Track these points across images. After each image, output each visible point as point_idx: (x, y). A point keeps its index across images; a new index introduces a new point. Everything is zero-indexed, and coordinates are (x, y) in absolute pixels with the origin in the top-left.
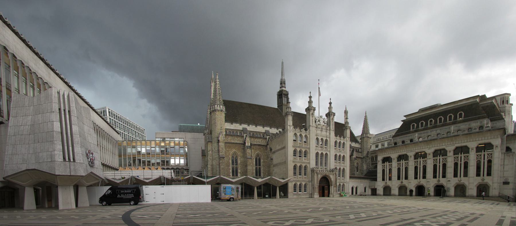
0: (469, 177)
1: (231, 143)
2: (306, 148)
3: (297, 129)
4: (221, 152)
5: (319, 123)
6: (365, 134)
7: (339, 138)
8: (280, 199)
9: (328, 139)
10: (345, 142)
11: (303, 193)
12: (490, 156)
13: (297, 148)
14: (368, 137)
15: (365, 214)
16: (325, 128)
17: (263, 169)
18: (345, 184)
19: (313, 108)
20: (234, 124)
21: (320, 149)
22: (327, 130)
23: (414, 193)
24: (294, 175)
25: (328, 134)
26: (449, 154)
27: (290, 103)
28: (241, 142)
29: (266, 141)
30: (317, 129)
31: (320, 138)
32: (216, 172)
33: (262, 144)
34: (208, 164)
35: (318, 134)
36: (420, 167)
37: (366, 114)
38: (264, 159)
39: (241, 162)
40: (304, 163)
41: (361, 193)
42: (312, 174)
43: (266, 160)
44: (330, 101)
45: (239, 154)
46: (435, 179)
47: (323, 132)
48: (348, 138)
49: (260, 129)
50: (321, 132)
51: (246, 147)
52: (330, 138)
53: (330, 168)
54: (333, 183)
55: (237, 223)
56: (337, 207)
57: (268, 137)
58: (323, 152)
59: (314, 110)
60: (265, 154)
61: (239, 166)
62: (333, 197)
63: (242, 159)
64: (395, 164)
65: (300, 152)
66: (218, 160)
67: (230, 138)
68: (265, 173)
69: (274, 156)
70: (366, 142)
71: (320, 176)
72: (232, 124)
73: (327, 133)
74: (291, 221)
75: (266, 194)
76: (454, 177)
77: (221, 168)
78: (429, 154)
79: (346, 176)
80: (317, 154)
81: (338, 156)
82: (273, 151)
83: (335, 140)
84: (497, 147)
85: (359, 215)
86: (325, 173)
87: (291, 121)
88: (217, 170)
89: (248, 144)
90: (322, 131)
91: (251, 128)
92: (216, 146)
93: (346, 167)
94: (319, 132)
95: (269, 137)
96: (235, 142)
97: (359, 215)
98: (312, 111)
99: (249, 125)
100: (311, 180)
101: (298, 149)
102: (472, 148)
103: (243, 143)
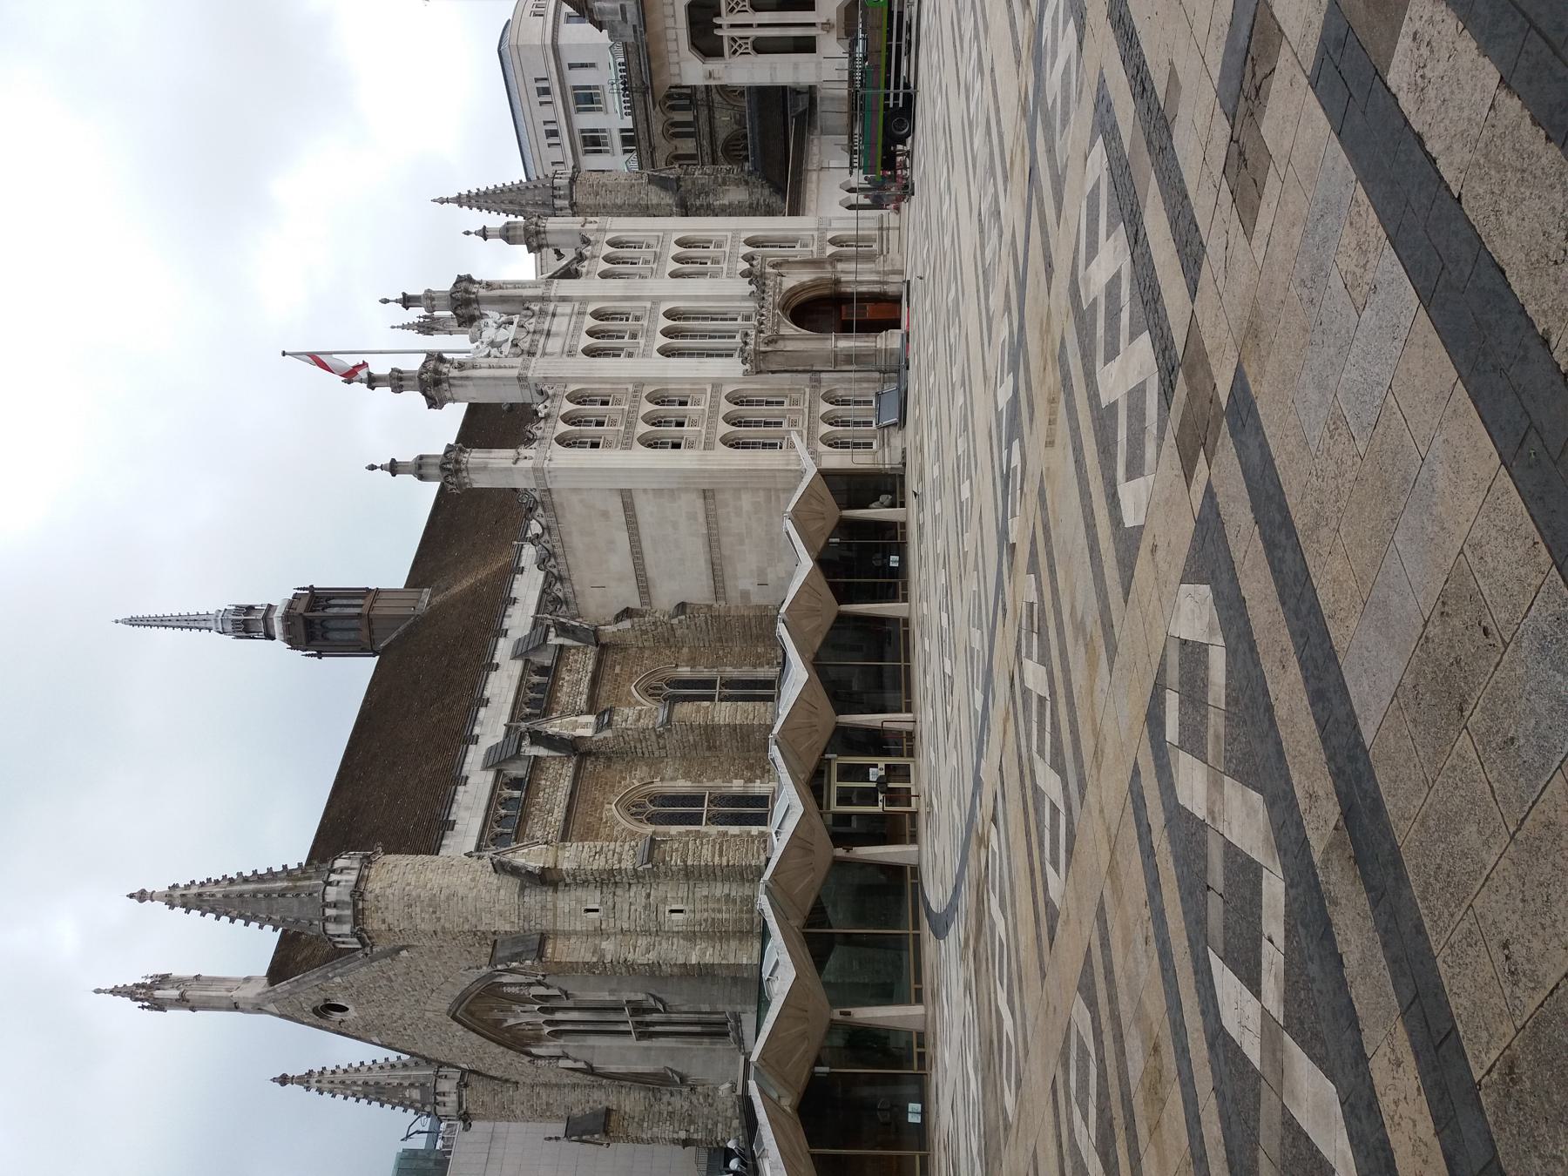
1: (567, 820)
2: (635, 396)
3: (534, 430)
5: (506, 348)
6: (554, 197)
7: (586, 263)
9: (591, 308)
10: (609, 236)
13: (641, 414)
14: (573, 180)
16: (533, 320)
18: (830, 235)
19: (431, 365)
21: (641, 341)
22: (543, 313)
24: (781, 448)
25: (565, 308)
27: (393, 460)
28: (569, 770)
29: (573, 651)
30: (539, 352)
33: (590, 668)
34: (681, 961)
35: (566, 349)
36: (760, 25)
37: (447, 201)
39: (686, 776)
40: (714, 407)
42: (774, 368)
43: (685, 650)
44: (396, 301)
45: (635, 780)
46: (820, 44)
47: (554, 329)
48: (588, 226)
49: (502, 685)
50: (557, 335)
51: (601, 735)
52: (585, 300)
53: (743, 298)
54: (827, 273)
55: (1042, 864)
56: (965, 554)
57: (553, 640)
58: (661, 328)
59: (439, 358)
60: (647, 653)
63: (669, 772)
65: (657, 422)
68: (758, 656)
70: (597, 194)
71: (789, 329)
73: (559, 310)
74: (1040, 782)
75: (879, 563)
79: (790, 233)
80: (666, 352)
81: (668, 340)
82: (635, 603)
83: (597, 277)
86: (772, 312)
87: (492, 455)
89: (585, 726)
90: (549, 331)
91: (492, 726)
92: (578, 901)
93: (737, 231)
94: (554, 345)
95: (552, 635)
96: (563, 805)
98: (445, 370)
99: (475, 740)
100: (807, 376)
101: (642, 428)
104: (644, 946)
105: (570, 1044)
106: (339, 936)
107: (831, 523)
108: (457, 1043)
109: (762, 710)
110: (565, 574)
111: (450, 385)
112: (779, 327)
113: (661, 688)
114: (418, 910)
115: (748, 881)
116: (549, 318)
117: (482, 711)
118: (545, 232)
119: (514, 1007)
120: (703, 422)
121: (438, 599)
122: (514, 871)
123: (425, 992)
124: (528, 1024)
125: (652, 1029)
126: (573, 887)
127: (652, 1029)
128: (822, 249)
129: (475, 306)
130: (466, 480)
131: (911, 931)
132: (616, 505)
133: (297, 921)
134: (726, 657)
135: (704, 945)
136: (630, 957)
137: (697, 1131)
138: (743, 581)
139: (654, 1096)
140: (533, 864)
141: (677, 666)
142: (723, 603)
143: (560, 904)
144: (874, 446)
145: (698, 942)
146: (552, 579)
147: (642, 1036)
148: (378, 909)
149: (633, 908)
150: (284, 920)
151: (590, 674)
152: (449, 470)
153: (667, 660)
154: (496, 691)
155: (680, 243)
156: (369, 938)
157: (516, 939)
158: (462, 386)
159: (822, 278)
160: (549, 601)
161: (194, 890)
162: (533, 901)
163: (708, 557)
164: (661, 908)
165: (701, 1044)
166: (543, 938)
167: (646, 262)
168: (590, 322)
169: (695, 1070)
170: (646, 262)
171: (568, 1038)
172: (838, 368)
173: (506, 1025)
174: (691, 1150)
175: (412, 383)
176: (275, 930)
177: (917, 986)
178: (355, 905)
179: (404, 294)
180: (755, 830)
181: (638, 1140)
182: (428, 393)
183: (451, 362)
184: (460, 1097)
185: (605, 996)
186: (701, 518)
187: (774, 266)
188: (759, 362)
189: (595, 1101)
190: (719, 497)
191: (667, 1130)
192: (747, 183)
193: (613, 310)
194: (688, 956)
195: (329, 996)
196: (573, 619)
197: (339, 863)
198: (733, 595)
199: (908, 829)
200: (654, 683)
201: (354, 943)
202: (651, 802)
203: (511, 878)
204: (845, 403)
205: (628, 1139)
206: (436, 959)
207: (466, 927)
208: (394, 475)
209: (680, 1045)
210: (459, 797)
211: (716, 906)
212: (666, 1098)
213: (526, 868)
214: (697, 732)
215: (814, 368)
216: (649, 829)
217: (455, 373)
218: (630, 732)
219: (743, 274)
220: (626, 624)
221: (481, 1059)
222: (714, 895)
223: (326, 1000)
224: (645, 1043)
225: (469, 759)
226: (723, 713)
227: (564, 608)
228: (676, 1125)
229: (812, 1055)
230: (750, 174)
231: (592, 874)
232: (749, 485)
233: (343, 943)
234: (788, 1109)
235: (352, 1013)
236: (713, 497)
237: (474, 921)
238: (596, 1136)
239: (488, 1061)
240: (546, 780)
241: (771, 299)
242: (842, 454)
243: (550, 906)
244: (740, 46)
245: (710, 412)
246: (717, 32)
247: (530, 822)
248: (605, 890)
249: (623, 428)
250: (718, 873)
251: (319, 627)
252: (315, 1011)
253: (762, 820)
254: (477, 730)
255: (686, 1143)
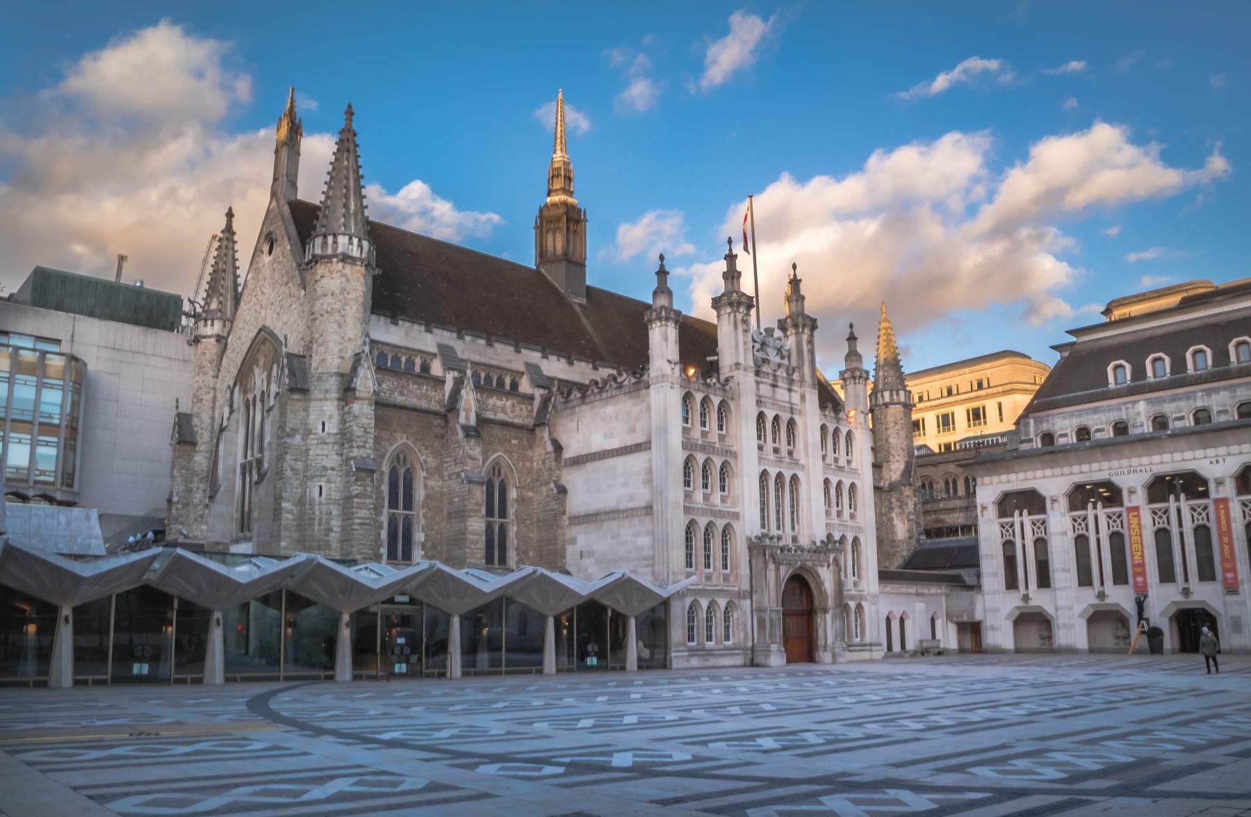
0: (1055, 590)
2: (726, 452)
4: (359, 447)
5: (760, 355)
6: (891, 392)
7: (832, 414)
8: (83, 693)
11: (721, 646)
12: (1200, 514)
15: (761, 746)
16: (785, 375)
17: (517, 533)
19: (743, 299)
20: (404, 325)
22: (791, 382)
23: (442, 670)
25: (796, 398)
26: (1217, 492)
28: (434, 406)
29: (529, 408)
30: (759, 379)
31: (770, 415)
32: (327, 535)
34: (284, 495)
35: (763, 399)
38: (523, 487)
40: (720, 514)
41: (925, 645)
42: (754, 562)
44: (795, 275)
46: (1013, 593)
47: (778, 390)
50: (774, 392)
58: (783, 471)
61: (421, 515)
62: (834, 662)
64: (1059, 522)
66: (338, 480)
67: (389, 383)
68: (526, 553)
69: (574, 480)
70: (896, 423)
71: (785, 572)
72: (431, 332)
73: (793, 394)
76: (1081, 584)
77: (357, 521)
78: (1219, 483)
80: (764, 475)
82: (568, 454)
83: (822, 423)
84: (1054, 501)
85: (783, 743)
88: (330, 530)
89: (467, 418)
90: (777, 386)
92: (331, 417)
94: (765, 390)
97: (783, 743)
98: (741, 310)
99: (460, 337)
102: (1051, 497)
103: (442, 410)
104: (296, 467)
105: (240, 415)
106: (314, 246)
107: (622, 608)
108: (245, 333)
109: (478, 556)
110: (587, 400)
111: (729, 314)
112: (787, 564)
113: (499, 475)
114: (330, 301)
115: (342, 546)
116: (787, 386)
117: (482, 342)
118: (855, 383)
119: (265, 373)
120: (707, 505)
121: (578, 309)
122: (354, 369)
123: (278, 308)
124: (255, 383)
125: (247, 475)
126: (342, 413)
127: (247, 475)
128: (853, 598)
129: (794, 332)
130: (654, 326)
131: (282, 674)
132: (639, 438)
133: (325, 216)
134: (525, 526)
135: (295, 512)
136: (288, 457)
137: (177, 509)
138: (583, 540)
139: (203, 478)
140: (358, 383)
141: (517, 488)
142: (567, 523)
143: (329, 403)
144: (690, 644)
145: (298, 508)
146: (582, 388)
147: (243, 467)
148: (331, 272)
149: (324, 458)
150: (327, 207)
151: (510, 420)
152: (661, 313)
153: (522, 480)
154: (499, 351)
155: (853, 486)
156: (311, 267)
157: (305, 372)
158: (729, 322)
159: (826, 598)
160: (568, 388)
161: (351, 147)
162: (331, 383)
163: (602, 511)
164: (324, 479)
165: (237, 511)
166: (304, 391)
167: (836, 460)
168: (785, 417)
169: (219, 507)
170: (836, 460)
171: (245, 413)
172: (755, 613)
173: (255, 367)
174: (165, 505)
175: (730, 286)
176: (321, 202)
177: (189, 680)
178: (335, 256)
179: (800, 280)
180: (384, 551)
181: (173, 466)
182: (723, 298)
183: (748, 314)
184: (210, 337)
185: (267, 439)
186: (632, 505)
187: (835, 560)
188: (758, 548)
189: (202, 434)
190: (647, 519)
191: (179, 487)
192: (910, 538)
193: (796, 434)
194: (288, 500)
195: (278, 242)
196: (554, 407)
197: (365, 244)
198: (571, 532)
199: (364, 672)
200: (503, 471)
201: (308, 257)
202: (408, 469)
203: (350, 366)
204: (727, 619)
205: (175, 458)
206: (299, 315)
207: (317, 336)
208: (657, 273)
209: (236, 496)
210: (416, 327)
211: (324, 521)
212: (202, 486)
213: (355, 376)
214: (461, 504)
215: (754, 594)
216: (386, 468)
217: (739, 317)
218: (461, 452)
219: (829, 536)
220: (550, 448)
221: (234, 351)
222: (331, 519)
223: (276, 240)
224: (238, 470)
225: (446, 333)
226: (476, 525)
227: (562, 400)
228: (183, 494)
229: (186, 596)
230: (918, 541)
231: (350, 426)
232: (656, 543)
233: (309, 249)
234: (145, 577)
235: (266, 259)
236: (646, 514)
237: (320, 341)
238: (177, 436)
239: (232, 356)
240: (427, 390)
241: (809, 558)
242: (683, 617)
243: (328, 396)
244: (1007, 531)
245: (716, 511)
246: (1017, 513)
247: (393, 379)
248: (338, 436)
249: (700, 442)
250: (348, 523)
251: (556, 226)
252: (270, 233)
253: (404, 559)
254: (468, 338)
255: (169, 501)
